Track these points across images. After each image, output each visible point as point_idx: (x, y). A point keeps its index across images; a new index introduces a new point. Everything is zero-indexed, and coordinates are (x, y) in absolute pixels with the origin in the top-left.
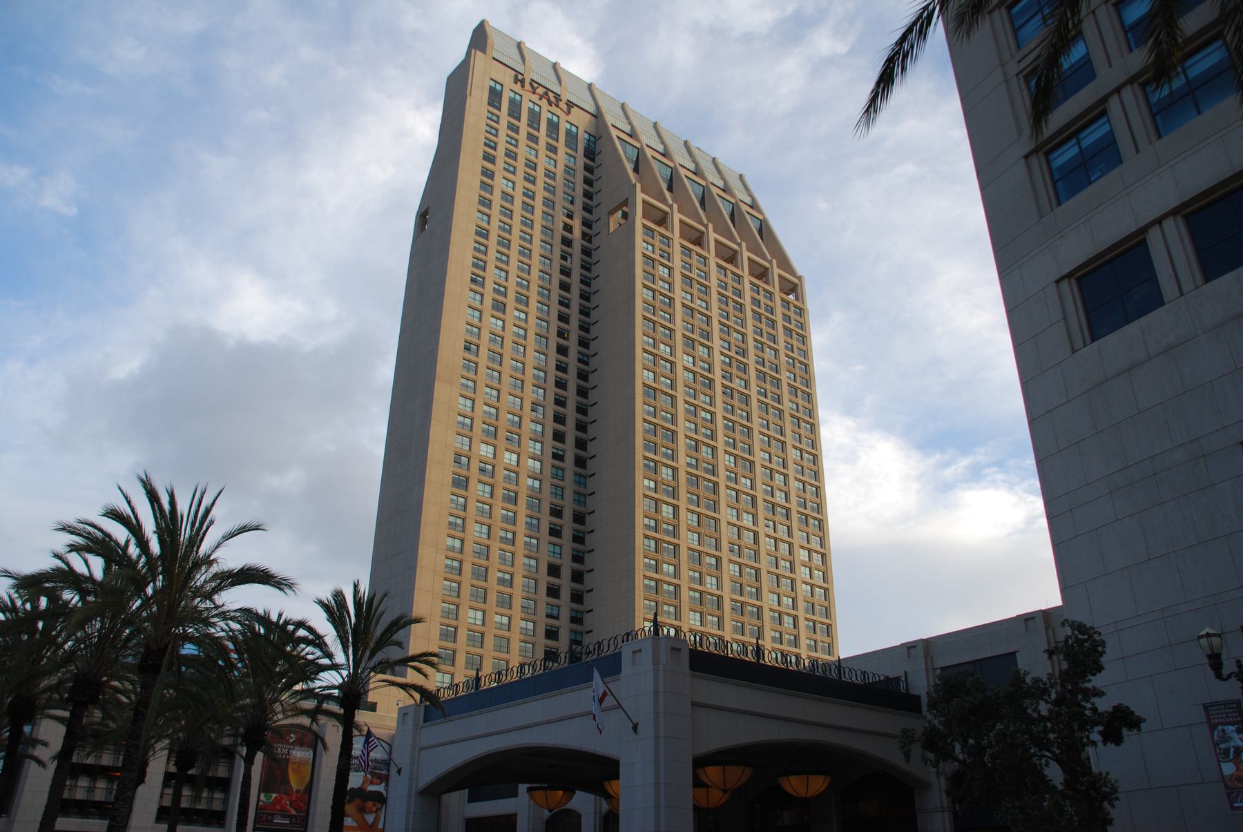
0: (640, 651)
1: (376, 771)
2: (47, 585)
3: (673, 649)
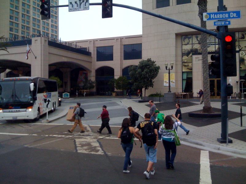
0: (37, 40)
1: (33, 135)
2: (36, 135)
3: (45, 40)
